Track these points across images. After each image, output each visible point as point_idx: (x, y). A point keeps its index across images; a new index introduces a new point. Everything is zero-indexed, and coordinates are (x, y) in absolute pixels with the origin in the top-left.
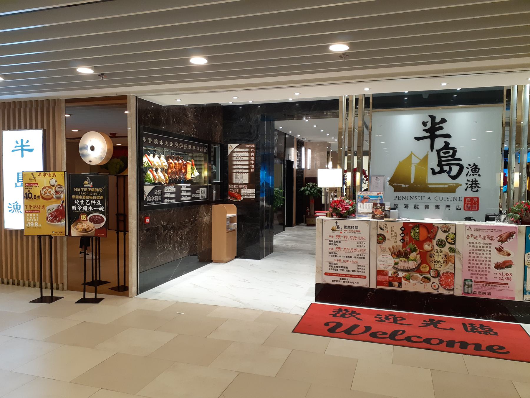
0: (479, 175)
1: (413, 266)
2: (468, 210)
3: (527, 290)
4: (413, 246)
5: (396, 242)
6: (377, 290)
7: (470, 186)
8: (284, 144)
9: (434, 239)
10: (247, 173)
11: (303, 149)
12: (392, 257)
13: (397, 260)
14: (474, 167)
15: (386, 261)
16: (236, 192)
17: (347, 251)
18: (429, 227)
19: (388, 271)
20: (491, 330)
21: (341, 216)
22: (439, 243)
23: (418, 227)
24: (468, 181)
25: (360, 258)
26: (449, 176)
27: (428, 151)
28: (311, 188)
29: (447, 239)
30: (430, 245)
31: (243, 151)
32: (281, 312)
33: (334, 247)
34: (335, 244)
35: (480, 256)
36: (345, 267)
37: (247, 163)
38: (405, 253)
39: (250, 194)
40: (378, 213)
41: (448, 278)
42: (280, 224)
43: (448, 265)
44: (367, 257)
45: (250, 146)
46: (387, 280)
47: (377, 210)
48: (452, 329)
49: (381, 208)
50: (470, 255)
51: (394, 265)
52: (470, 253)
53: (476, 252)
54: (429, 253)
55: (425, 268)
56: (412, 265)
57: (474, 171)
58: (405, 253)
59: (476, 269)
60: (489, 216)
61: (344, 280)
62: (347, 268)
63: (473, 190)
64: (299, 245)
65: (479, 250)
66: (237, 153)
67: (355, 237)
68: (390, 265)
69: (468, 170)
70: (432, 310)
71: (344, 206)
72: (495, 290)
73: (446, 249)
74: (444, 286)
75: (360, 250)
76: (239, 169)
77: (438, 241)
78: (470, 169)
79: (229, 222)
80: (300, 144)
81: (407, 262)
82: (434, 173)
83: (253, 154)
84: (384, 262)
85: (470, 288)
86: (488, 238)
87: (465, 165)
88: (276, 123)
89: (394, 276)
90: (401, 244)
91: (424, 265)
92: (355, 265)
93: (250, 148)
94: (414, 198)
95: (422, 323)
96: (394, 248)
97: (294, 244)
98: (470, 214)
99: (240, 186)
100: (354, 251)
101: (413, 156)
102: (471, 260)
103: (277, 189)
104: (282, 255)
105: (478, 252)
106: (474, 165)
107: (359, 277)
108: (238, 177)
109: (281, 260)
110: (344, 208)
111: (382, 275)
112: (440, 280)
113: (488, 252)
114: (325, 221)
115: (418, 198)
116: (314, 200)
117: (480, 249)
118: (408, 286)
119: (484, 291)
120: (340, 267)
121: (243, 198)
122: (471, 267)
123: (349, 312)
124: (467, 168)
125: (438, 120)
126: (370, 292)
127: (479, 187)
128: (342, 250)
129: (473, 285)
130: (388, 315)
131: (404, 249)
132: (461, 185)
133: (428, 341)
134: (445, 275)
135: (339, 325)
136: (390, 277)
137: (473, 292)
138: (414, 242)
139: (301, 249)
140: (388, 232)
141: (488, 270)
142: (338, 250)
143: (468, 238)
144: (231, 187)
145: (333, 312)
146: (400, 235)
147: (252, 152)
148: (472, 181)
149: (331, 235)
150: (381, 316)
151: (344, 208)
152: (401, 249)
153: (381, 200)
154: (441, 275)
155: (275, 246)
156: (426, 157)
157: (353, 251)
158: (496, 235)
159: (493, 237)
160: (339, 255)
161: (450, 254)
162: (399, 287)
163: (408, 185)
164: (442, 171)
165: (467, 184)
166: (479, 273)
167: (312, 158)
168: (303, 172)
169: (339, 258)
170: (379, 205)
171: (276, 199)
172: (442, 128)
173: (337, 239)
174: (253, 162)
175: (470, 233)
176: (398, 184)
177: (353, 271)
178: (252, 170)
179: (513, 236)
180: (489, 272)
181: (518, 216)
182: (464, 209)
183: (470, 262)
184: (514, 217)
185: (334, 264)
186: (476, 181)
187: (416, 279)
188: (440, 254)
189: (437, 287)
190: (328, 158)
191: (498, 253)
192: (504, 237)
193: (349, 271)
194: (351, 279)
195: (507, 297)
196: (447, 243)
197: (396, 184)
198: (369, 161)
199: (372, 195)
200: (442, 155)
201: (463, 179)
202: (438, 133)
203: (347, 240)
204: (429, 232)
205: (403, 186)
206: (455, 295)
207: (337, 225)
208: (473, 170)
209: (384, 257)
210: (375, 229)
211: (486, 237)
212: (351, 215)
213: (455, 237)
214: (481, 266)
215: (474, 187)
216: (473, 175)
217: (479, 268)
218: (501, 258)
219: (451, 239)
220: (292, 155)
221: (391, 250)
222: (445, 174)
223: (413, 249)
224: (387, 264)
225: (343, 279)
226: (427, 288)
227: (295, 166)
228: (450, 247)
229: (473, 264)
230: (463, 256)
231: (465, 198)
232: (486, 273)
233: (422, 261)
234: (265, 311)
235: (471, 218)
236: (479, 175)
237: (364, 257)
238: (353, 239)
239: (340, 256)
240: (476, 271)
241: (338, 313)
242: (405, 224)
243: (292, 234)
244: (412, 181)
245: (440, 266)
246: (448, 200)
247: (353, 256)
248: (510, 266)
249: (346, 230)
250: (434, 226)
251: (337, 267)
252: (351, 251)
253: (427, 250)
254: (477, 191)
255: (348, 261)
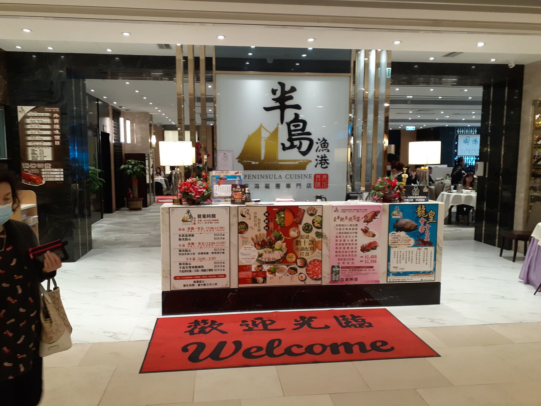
0: (328, 151)
1: (278, 257)
2: (318, 188)
3: (391, 271)
4: (278, 233)
5: (259, 230)
6: (240, 289)
7: (319, 162)
8: (96, 113)
9: (300, 223)
10: (50, 146)
11: (122, 120)
12: (255, 249)
13: (261, 251)
14: (324, 142)
15: (249, 253)
16: (33, 174)
17: (203, 246)
18: (294, 211)
19: (251, 265)
20: (363, 320)
21: (193, 202)
22: (305, 228)
23: (283, 211)
24: (318, 157)
25: (218, 253)
26: (299, 151)
27: (278, 124)
28: (134, 165)
29: (313, 223)
30: (297, 231)
31: (42, 117)
32: (118, 341)
33: (186, 243)
34: (186, 239)
35: (346, 239)
36: (200, 267)
37: (49, 133)
38: (270, 243)
39: (56, 176)
40: (237, 197)
41: (316, 266)
42: (97, 211)
43: (315, 252)
44: (227, 251)
45: (52, 110)
46: (251, 276)
47: (236, 193)
48: (327, 327)
49: (241, 190)
50: (337, 239)
51: (258, 257)
52: (337, 237)
53: (343, 235)
54: (295, 240)
55: (291, 258)
56: (277, 255)
57: (323, 146)
58: (270, 243)
59: (343, 254)
60: (350, 195)
61: (199, 283)
62: (202, 267)
63: (323, 166)
64: (125, 236)
65: (345, 233)
66: (33, 119)
67: (212, 228)
68: (253, 258)
69: (318, 145)
70: (300, 304)
71: (197, 189)
72: (361, 274)
73: (312, 235)
74: (312, 276)
75: (218, 243)
76: (37, 141)
77: (305, 225)
78: (319, 144)
79: (25, 215)
80: (116, 115)
81: (272, 252)
82: (284, 148)
83: (56, 121)
84: (246, 255)
85: (337, 275)
86: (354, 219)
87: (315, 140)
88: (88, 82)
89: (258, 270)
90: (265, 232)
91: (290, 254)
92: (213, 262)
93: (52, 113)
94: (265, 177)
95: (295, 324)
96: (258, 237)
97: (118, 235)
98: (320, 192)
99: (40, 166)
100: (211, 245)
101: (263, 130)
102: (338, 244)
103: (93, 168)
104: (105, 251)
105: (345, 235)
106: (324, 139)
107: (217, 276)
108: (36, 152)
109: (104, 260)
110: (196, 192)
111: (244, 271)
112: (307, 270)
113: (355, 235)
114: (173, 210)
115: (268, 176)
116: (137, 180)
117: (347, 231)
118: (273, 281)
119: (351, 277)
120: (194, 267)
121: (46, 181)
122: (338, 252)
123: (208, 323)
124: (317, 143)
125: (287, 88)
126: (231, 293)
127: (328, 164)
128: (196, 245)
129: (340, 271)
130: (255, 319)
131: (269, 238)
132: (310, 161)
133: (310, 349)
134: (313, 264)
135: (201, 347)
136: (253, 272)
137: (340, 279)
138: (279, 229)
139: (127, 241)
140: (250, 219)
141: (354, 254)
142: (191, 246)
143: (335, 220)
144: (25, 166)
145: (189, 327)
146: (264, 221)
147: (55, 118)
148: (322, 157)
149: (182, 228)
150: (247, 322)
151: (196, 192)
152: (265, 238)
153: (240, 180)
154: (309, 264)
155: (96, 240)
156: (276, 130)
157: (209, 246)
158: (362, 215)
159: (358, 218)
160: (192, 252)
161: (317, 239)
162: (263, 283)
163: (258, 163)
164: (292, 147)
165: (316, 160)
166: (346, 258)
167: (132, 131)
168: (121, 147)
169: (192, 256)
170: (238, 187)
171: (93, 181)
172: (291, 98)
173: (190, 233)
174: (57, 132)
175: (336, 215)
176: (248, 161)
177: (210, 270)
178: (57, 143)
179: (377, 215)
180: (356, 256)
181: (382, 194)
182: (315, 187)
183: (337, 246)
184: (378, 195)
185: (187, 264)
186: (325, 157)
187: (282, 271)
188: (307, 240)
189: (304, 278)
190: (150, 132)
191: (364, 234)
192: (369, 216)
193: (205, 270)
194: (207, 281)
195: (372, 281)
196: (314, 228)
197: (245, 161)
198: (409, 102)
199: (229, 174)
200: (292, 128)
201: (313, 155)
202: (288, 103)
203: (201, 232)
204: (295, 216)
205: (253, 163)
206: (323, 284)
207: (189, 214)
208: (323, 145)
209: (246, 249)
210: (236, 217)
211: (353, 218)
212: (206, 200)
213: (322, 220)
214: (348, 250)
215: (323, 163)
216: (323, 150)
217: (346, 252)
218: (366, 240)
219: (317, 223)
220: (108, 125)
221: (254, 240)
222: (296, 150)
223: (278, 237)
224: (250, 258)
225: (198, 282)
226: (294, 281)
227: (112, 140)
228: (317, 232)
229: (340, 248)
230: (330, 240)
231: (315, 176)
232: (353, 257)
233: (288, 250)
234: (93, 343)
235: (322, 197)
236: (328, 151)
237: (223, 251)
238: (210, 231)
239: (194, 254)
240: (343, 256)
241: (195, 327)
242: (270, 209)
243: (113, 222)
244: (262, 158)
245: (307, 254)
246: (299, 177)
247: (210, 252)
248: (375, 248)
249: (201, 221)
250: (300, 209)
251: (190, 267)
252: (207, 246)
253: (293, 237)
254: (327, 167)
255: (204, 259)
